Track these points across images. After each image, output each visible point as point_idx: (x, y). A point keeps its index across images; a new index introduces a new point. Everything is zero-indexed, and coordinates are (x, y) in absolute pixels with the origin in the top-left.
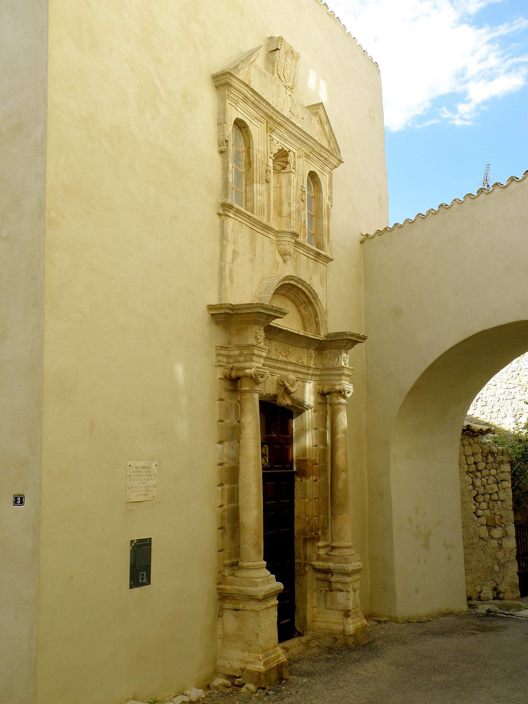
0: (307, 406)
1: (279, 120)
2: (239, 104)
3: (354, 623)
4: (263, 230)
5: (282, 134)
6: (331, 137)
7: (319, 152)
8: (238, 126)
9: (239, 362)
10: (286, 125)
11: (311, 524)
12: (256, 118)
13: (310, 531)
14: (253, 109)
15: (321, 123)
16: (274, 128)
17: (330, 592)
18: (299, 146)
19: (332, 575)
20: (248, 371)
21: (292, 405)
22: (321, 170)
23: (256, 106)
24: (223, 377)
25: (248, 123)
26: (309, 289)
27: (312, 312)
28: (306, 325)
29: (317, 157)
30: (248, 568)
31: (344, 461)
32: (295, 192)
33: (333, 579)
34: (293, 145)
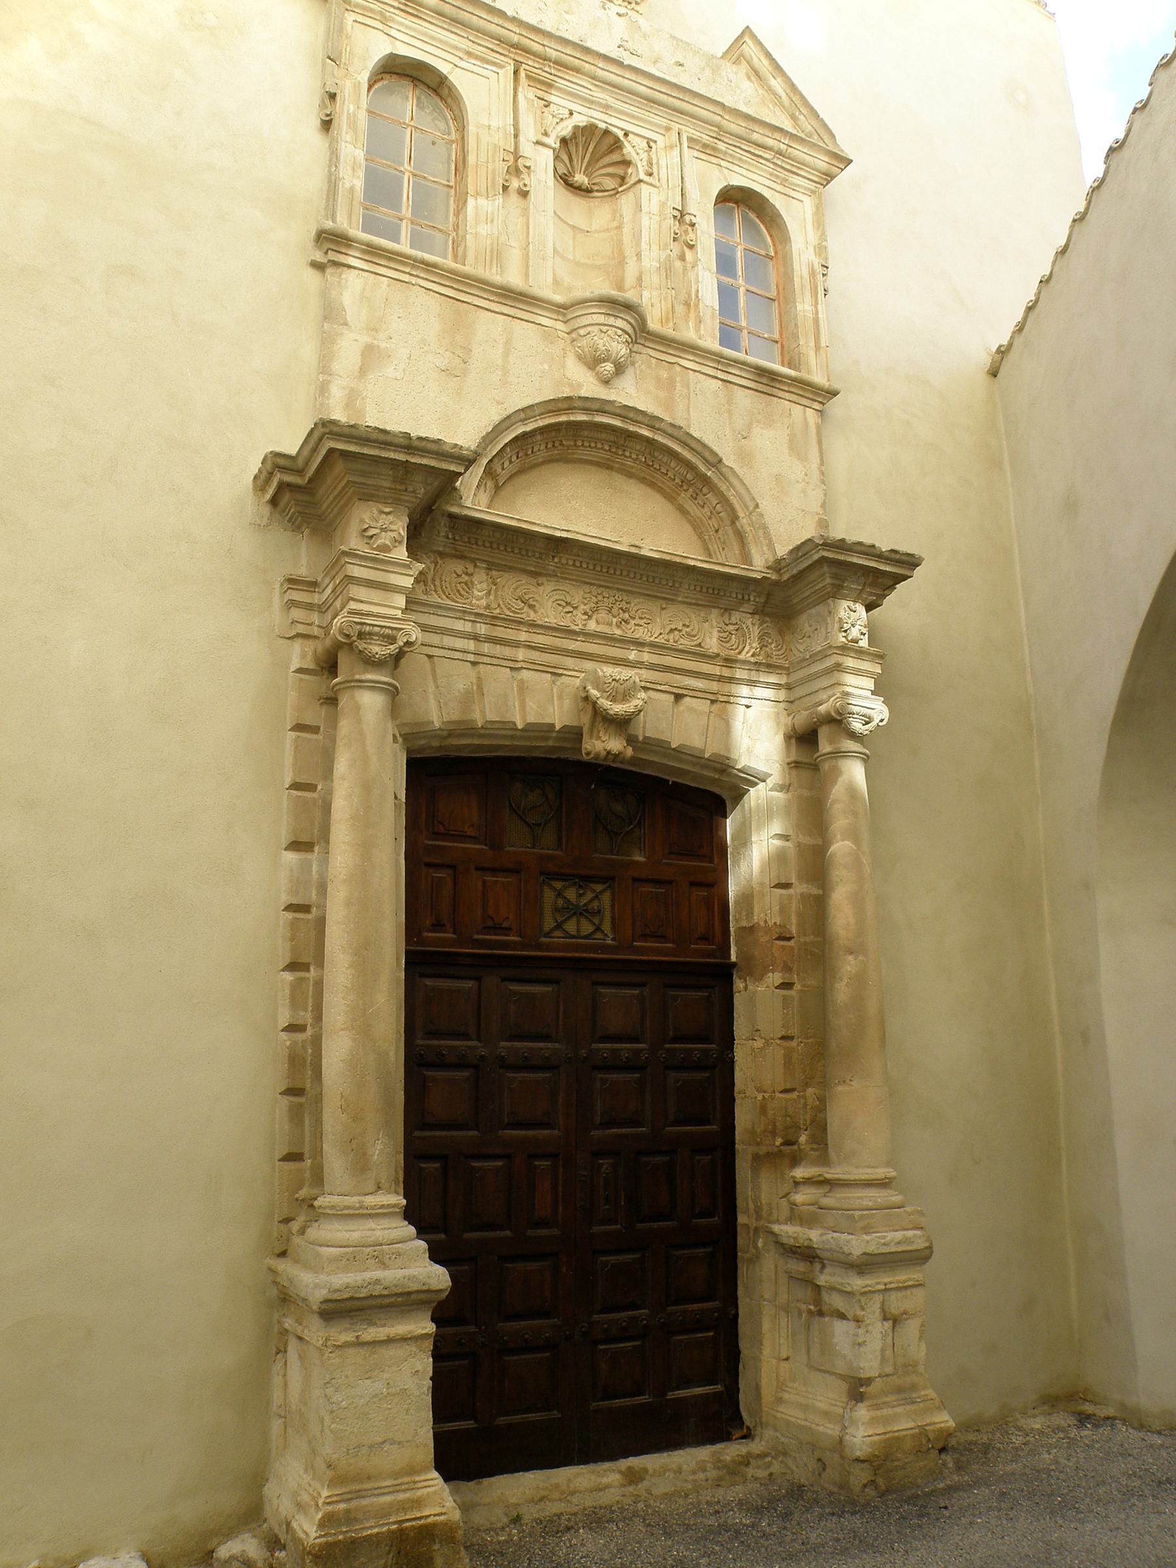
0: (739, 770)
1: (553, 54)
2: (393, 20)
3: (873, 1421)
4: (507, 305)
6: (798, 101)
7: (744, 135)
11: (770, 1113)
12: (469, 54)
13: (769, 1135)
14: (452, 32)
15: (759, 77)
17: (817, 1319)
18: (664, 122)
19: (823, 1267)
23: (455, 21)
24: (312, 666)
25: (444, 68)
26: (682, 439)
28: (710, 547)
29: (746, 151)
31: (852, 920)
34: (633, 117)
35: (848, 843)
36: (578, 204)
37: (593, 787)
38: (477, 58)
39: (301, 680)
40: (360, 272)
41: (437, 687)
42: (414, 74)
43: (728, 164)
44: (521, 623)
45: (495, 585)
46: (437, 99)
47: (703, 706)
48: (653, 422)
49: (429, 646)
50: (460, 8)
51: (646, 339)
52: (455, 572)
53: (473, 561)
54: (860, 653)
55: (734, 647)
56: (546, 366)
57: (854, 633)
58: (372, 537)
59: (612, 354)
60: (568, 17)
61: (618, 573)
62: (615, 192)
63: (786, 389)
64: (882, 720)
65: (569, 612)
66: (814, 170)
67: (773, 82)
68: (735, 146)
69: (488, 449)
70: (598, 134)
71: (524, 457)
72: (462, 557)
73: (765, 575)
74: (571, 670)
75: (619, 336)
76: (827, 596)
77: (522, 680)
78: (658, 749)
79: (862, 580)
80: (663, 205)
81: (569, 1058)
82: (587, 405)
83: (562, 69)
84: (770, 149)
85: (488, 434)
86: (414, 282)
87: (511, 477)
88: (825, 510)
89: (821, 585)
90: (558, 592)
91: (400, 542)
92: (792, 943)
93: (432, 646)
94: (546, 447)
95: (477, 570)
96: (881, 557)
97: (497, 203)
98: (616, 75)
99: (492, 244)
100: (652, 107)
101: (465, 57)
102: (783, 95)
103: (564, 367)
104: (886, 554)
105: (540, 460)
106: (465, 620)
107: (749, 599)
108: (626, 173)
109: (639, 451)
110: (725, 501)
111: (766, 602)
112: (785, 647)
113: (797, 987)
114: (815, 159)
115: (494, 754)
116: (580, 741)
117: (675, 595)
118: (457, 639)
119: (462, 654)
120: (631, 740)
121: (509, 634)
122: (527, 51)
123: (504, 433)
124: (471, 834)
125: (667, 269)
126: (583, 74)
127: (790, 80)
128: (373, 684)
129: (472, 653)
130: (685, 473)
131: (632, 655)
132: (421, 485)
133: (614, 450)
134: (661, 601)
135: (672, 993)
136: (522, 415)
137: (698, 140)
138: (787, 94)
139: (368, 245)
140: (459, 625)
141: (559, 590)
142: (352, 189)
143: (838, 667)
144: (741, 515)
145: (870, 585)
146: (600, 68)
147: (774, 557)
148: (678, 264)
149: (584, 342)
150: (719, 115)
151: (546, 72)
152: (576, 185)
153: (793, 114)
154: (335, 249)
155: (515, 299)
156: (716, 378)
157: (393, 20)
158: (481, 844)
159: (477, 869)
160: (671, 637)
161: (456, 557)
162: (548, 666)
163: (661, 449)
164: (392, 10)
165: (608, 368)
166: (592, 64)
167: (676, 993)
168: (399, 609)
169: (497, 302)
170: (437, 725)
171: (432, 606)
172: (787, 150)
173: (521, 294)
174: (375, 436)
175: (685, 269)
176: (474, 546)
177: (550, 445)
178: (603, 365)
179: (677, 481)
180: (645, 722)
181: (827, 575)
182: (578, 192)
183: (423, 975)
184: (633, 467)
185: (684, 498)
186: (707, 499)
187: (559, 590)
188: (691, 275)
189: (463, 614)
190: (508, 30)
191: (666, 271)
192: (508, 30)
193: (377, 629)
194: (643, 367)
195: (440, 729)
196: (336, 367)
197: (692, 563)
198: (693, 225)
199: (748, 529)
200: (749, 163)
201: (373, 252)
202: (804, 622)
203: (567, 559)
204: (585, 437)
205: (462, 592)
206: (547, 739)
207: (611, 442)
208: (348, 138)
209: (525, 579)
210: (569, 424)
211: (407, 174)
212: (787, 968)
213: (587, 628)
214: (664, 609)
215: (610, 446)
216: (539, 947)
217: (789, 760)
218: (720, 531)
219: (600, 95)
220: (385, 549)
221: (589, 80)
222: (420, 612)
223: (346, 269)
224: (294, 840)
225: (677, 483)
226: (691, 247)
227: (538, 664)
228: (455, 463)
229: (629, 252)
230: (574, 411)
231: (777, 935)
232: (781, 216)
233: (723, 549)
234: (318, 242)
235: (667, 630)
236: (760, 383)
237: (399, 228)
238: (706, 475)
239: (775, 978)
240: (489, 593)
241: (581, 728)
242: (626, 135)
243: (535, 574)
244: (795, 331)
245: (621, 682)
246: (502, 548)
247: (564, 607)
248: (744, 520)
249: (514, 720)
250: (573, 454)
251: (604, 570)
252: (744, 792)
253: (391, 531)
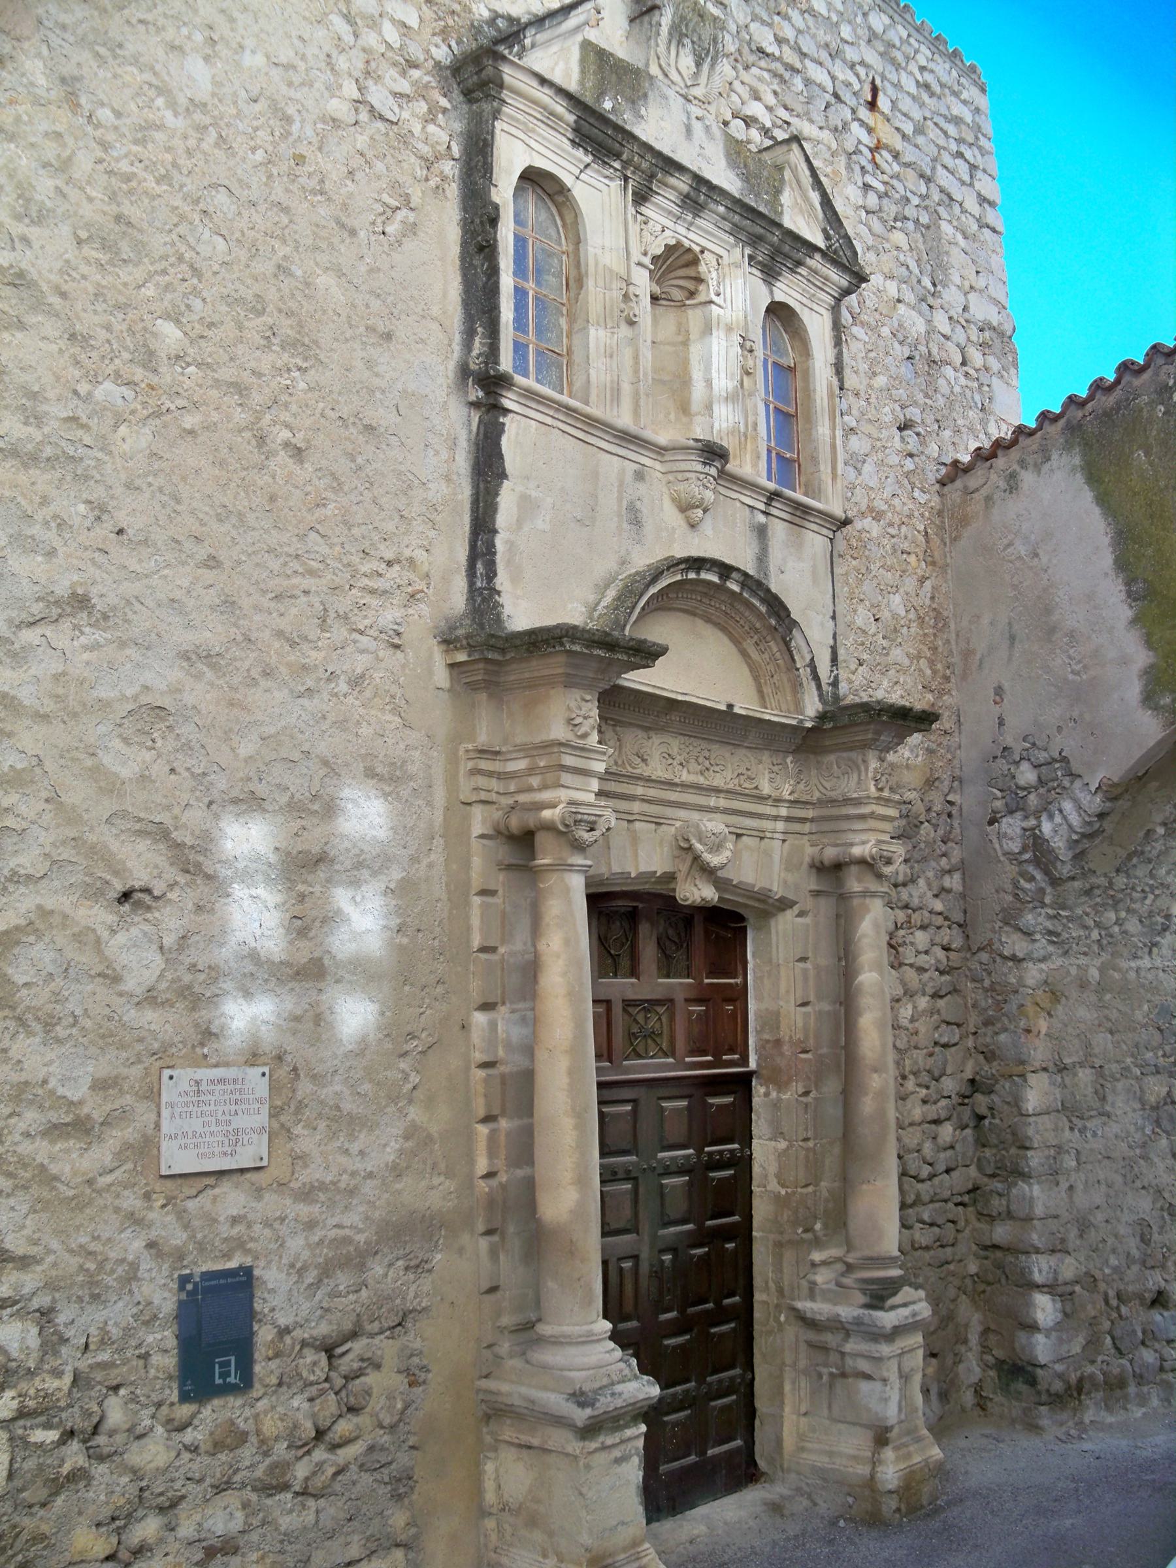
2: (533, 131)
9: (530, 789)
20: (547, 814)
22: (804, 300)
24: (491, 832)
25: (568, 180)
27: (778, 655)
30: (557, 1342)
31: (877, 1043)
32: (723, 353)
33: (849, 1347)
70: (681, 251)
157: (533, 131)
242: (702, 252)
243: (647, 729)
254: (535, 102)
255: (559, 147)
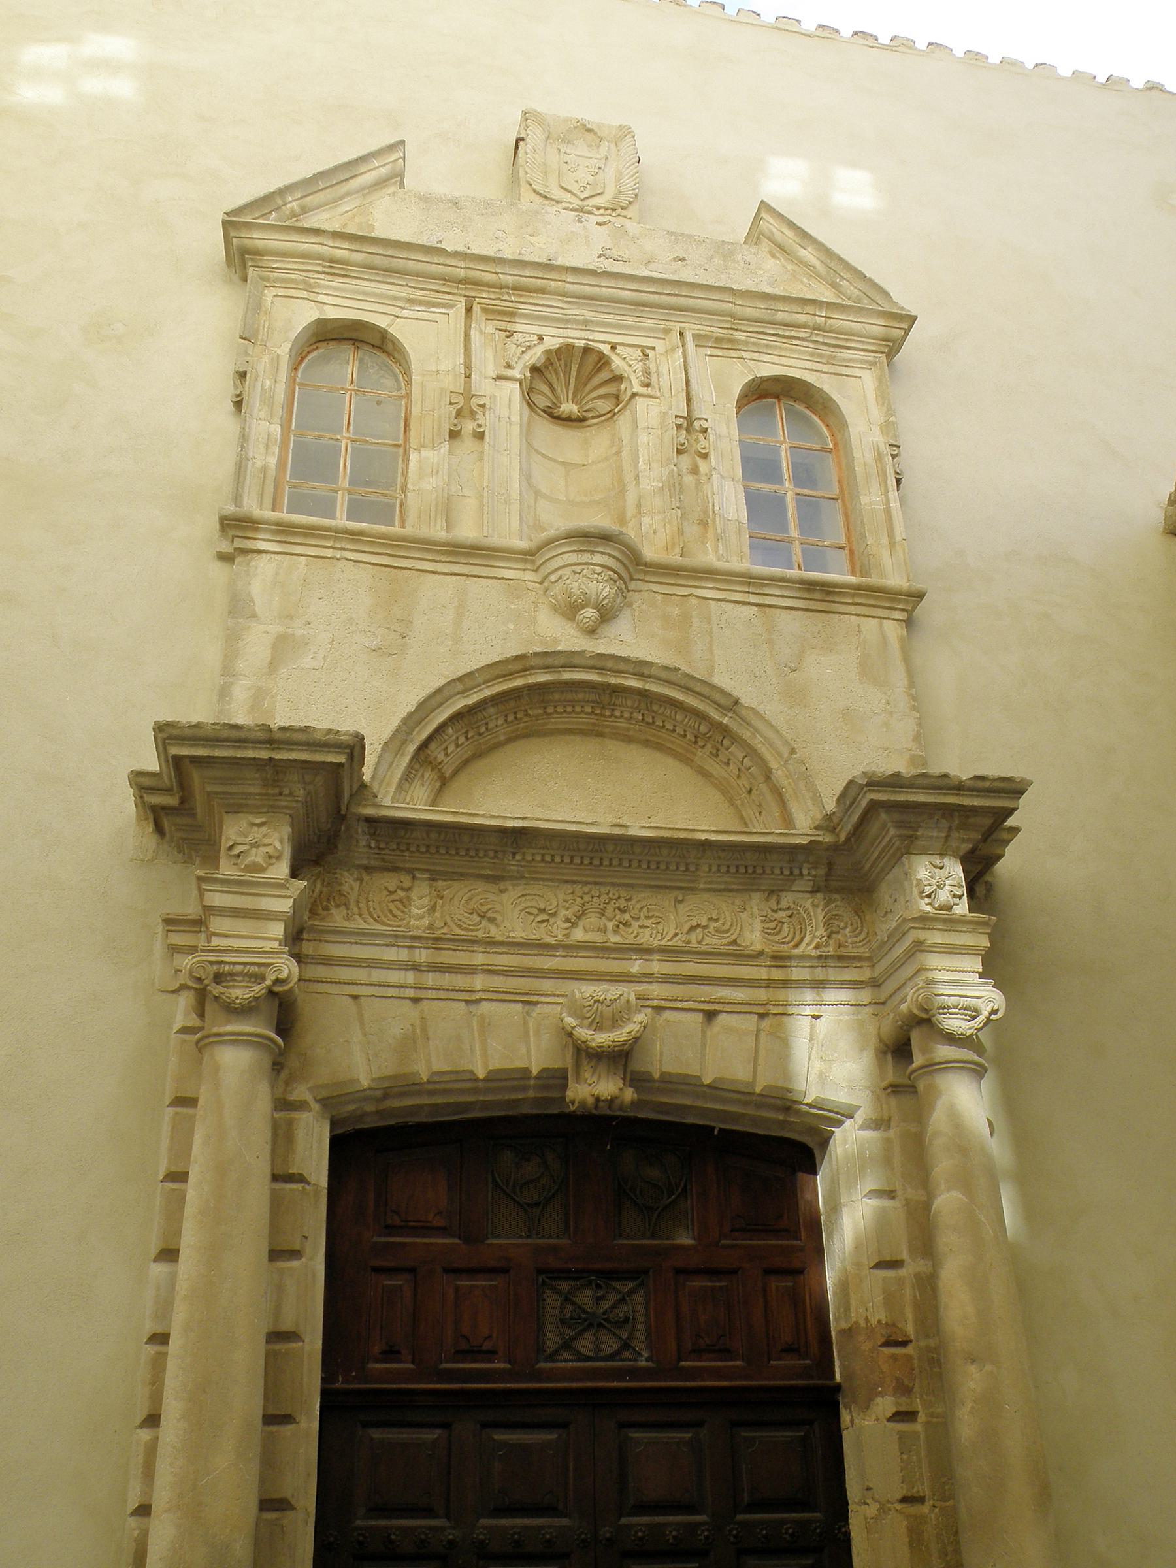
0: (809, 1105)
1: (510, 280)
2: (319, 286)
4: (459, 563)
5: (562, 311)
7: (767, 318)
8: (373, 346)
10: (552, 282)
12: (411, 301)
16: (511, 305)
18: (661, 325)
21: (639, 1099)
23: (388, 270)
25: (381, 322)
29: (773, 335)
35: (955, 1194)
36: (569, 437)
37: (608, 1147)
38: (420, 303)
39: (184, 1041)
40: (272, 556)
41: (365, 1035)
42: (354, 335)
43: (752, 354)
44: (473, 942)
45: (442, 898)
46: (384, 357)
47: (748, 1023)
48: (669, 675)
49: (353, 984)
50: (392, 257)
51: (645, 573)
52: (386, 888)
53: (411, 872)
54: (951, 923)
55: (787, 940)
56: (511, 626)
57: (944, 896)
58: (239, 855)
59: (590, 597)
60: (533, 239)
61: (606, 862)
62: (612, 413)
63: (850, 601)
64: (994, 1012)
65: (543, 921)
66: (868, 338)
67: (803, 253)
68: (757, 332)
69: (415, 733)
70: (578, 355)
71: (477, 737)
72: (395, 869)
73: (813, 838)
74: (550, 995)
75: (598, 574)
76: (899, 854)
77: (482, 1016)
78: (683, 1087)
79: (944, 823)
80: (664, 415)
81: (584, 1541)
82: (570, 660)
83: (524, 293)
84: (803, 326)
85: (410, 715)
86: (338, 557)
87: (466, 763)
88: (920, 743)
89: (887, 839)
90: (528, 897)
91: (279, 858)
92: (909, 1350)
93: (357, 984)
94: (506, 720)
95: (417, 883)
96: (959, 788)
97: (442, 451)
98: (590, 285)
99: (437, 497)
100: (642, 311)
101: (407, 306)
102: (817, 264)
103: (534, 622)
104: (968, 783)
105: (502, 738)
106: (398, 946)
107: (801, 874)
108: (619, 390)
109: (632, 707)
110: (752, 752)
111: (828, 875)
112: (865, 930)
113: (922, 1417)
114: (866, 325)
115: (435, 1120)
116: (565, 1087)
117: (693, 881)
118: (390, 971)
119: (397, 989)
120: (637, 1080)
121: (462, 958)
122: (477, 283)
123: (437, 711)
124: (439, 1224)
125: (674, 487)
126: (550, 293)
127: (823, 245)
128: (234, 1038)
129: (411, 987)
130: (696, 726)
131: (636, 967)
132: (299, 785)
133: (569, 709)
134: (677, 893)
135: (746, 1434)
136: (459, 687)
137: (707, 335)
138: (821, 261)
139: (278, 524)
140: (391, 954)
141: (529, 894)
142: (265, 468)
143: (919, 947)
144: (774, 765)
145: (958, 829)
146: (568, 282)
147: (822, 812)
148: (689, 479)
149: (556, 589)
150: (729, 302)
151: (505, 300)
152: (563, 416)
153: (833, 282)
154: (240, 535)
155: (468, 555)
156: (749, 604)
157: (319, 286)
158: (453, 1236)
159: (446, 1271)
160: (693, 937)
161: (388, 870)
162: (516, 993)
163: (659, 700)
164: (316, 276)
165: (588, 614)
166: (559, 281)
167: (751, 1435)
168: (275, 939)
169: (446, 562)
170: (365, 1083)
171: (351, 934)
172: (826, 323)
173: (472, 547)
174: (225, 733)
175: (699, 483)
176: (406, 854)
177: (511, 718)
178: (582, 612)
179: (688, 737)
180: (661, 1053)
181: (889, 824)
182: (570, 423)
183: (366, 1425)
184: (628, 729)
185: (701, 756)
186: (730, 753)
187: (529, 894)
188: (707, 488)
189: (394, 940)
190: (452, 266)
191: (670, 490)
192: (452, 266)
193: (239, 968)
194: (644, 607)
195: (370, 1089)
196: (241, 665)
197: (703, 837)
198: (705, 431)
199: (785, 782)
200: (780, 348)
201: (284, 530)
202: (884, 893)
203: (533, 855)
204: (556, 702)
205: (398, 913)
206: (524, 1089)
207: (592, 702)
208: (262, 415)
209: (480, 886)
210: (530, 688)
211: (344, 441)
212: (903, 1389)
213: (572, 938)
214: (681, 902)
215: (592, 707)
216: (538, 1376)
217: (884, 1084)
218: (754, 791)
219: (575, 312)
220: (255, 868)
221: (560, 298)
222: (338, 942)
223: (256, 555)
224: (164, 1247)
225: (689, 740)
226: (705, 456)
227: (503, 992)
228: (333, 752)
229: (628, 477)
230: (533, 672)
231: (883, 1340)
232: (831, 399)
233: (760, 813)
234: (223, 532)
235: (686, 927)
236: (811, 600)
237: (333, 503)
238: (722, 722)
239: (886, 1405)
240: (433, 909)
241: (565, 1070)
242: (613, 348)
243: (495, 879)
244: (862, 530)
245: (608, 1003)
246: (453, 852)
247: (537, 915)
248: (780, 772)
249: (471, 1068)
250: (546, 724)
251: (758, 872)
252: (829, 1135)
253: (265, 845)
254: (305, 256)
255: (354, 292)
